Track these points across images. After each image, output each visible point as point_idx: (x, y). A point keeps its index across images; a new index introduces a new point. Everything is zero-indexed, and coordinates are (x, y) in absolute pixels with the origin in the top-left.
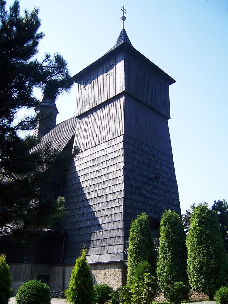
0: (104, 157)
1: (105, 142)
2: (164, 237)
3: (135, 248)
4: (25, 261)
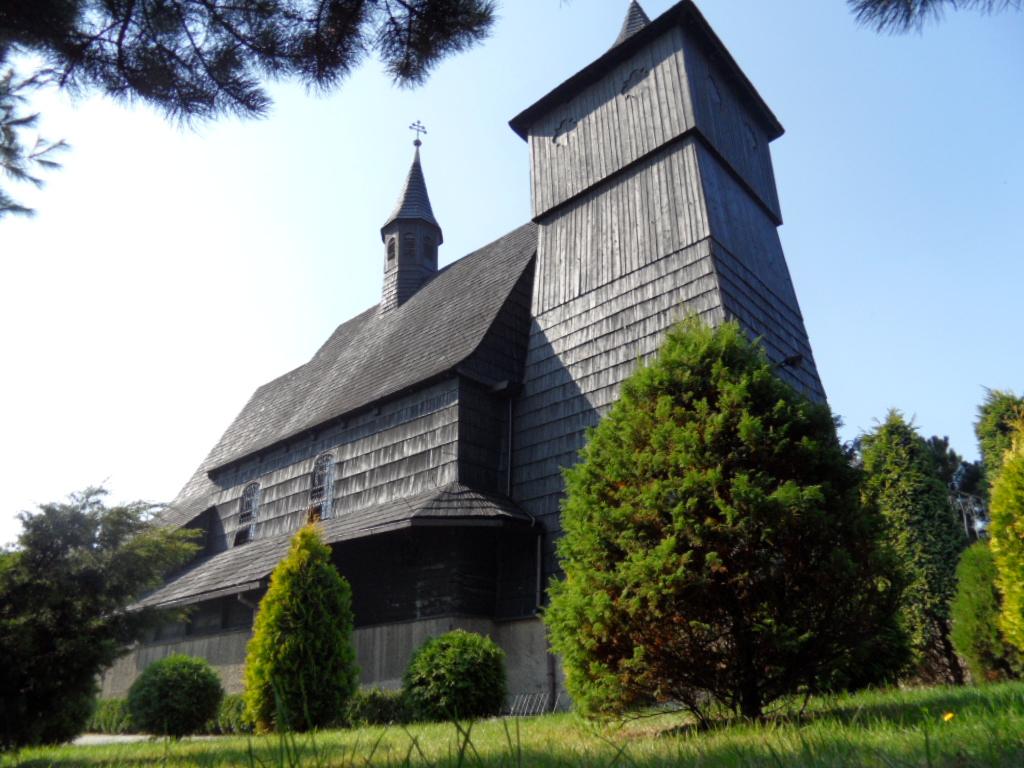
0: (650, 306)
1: (646, 266)
3: (903, 513)
4: (418, 613)
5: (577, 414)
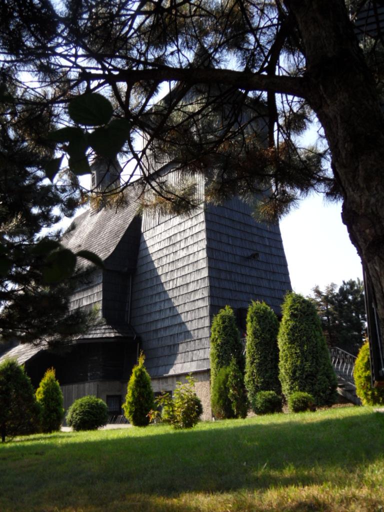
0: (182, 234)
2: (251, 336)
4: (89, 379)
5: (155, 286)
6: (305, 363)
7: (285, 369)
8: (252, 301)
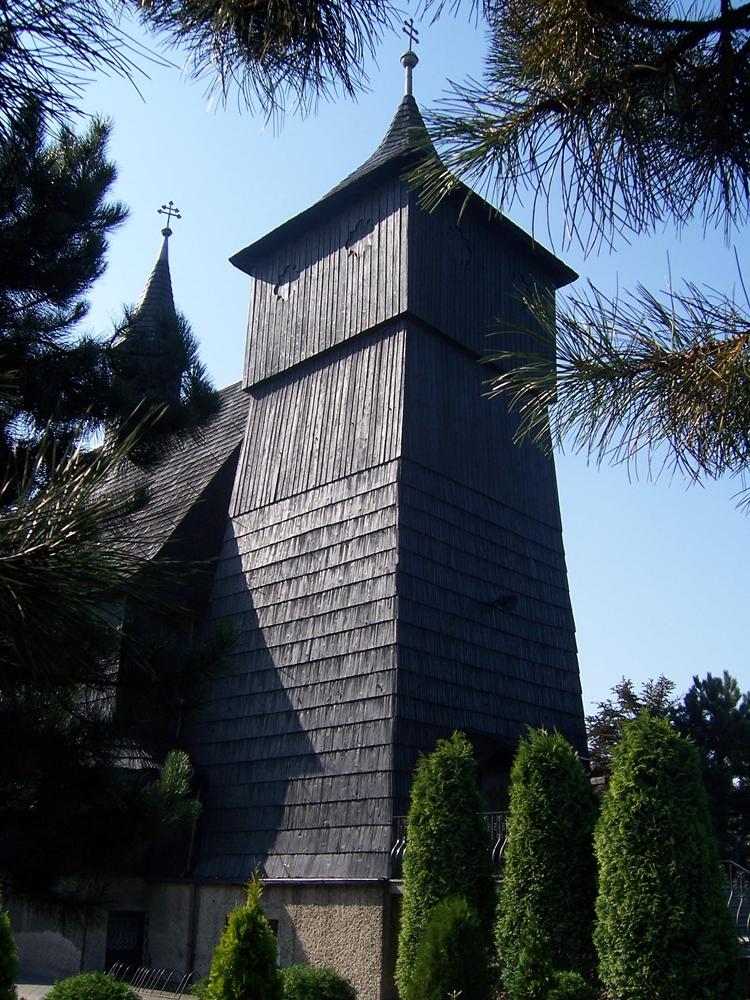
6: (671, 908)
7: (613, 918)
8: (529, 728)
